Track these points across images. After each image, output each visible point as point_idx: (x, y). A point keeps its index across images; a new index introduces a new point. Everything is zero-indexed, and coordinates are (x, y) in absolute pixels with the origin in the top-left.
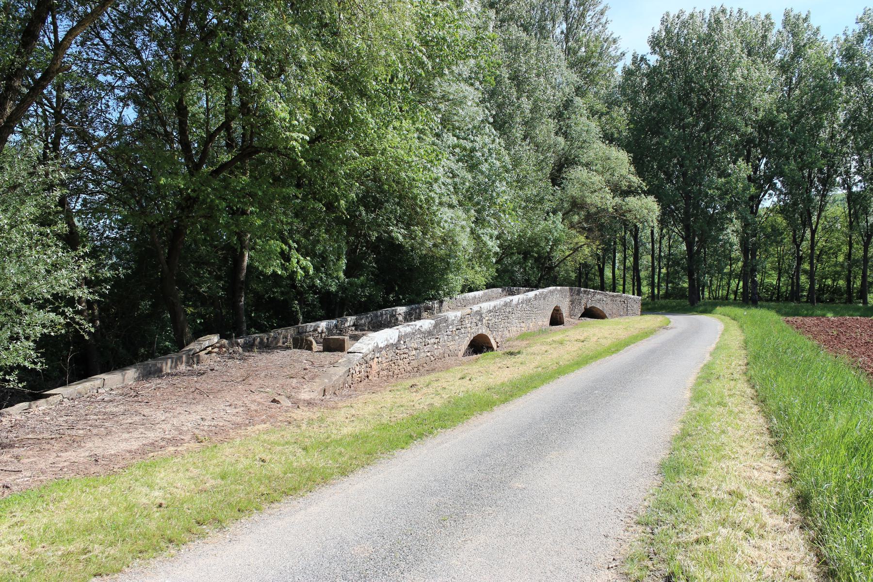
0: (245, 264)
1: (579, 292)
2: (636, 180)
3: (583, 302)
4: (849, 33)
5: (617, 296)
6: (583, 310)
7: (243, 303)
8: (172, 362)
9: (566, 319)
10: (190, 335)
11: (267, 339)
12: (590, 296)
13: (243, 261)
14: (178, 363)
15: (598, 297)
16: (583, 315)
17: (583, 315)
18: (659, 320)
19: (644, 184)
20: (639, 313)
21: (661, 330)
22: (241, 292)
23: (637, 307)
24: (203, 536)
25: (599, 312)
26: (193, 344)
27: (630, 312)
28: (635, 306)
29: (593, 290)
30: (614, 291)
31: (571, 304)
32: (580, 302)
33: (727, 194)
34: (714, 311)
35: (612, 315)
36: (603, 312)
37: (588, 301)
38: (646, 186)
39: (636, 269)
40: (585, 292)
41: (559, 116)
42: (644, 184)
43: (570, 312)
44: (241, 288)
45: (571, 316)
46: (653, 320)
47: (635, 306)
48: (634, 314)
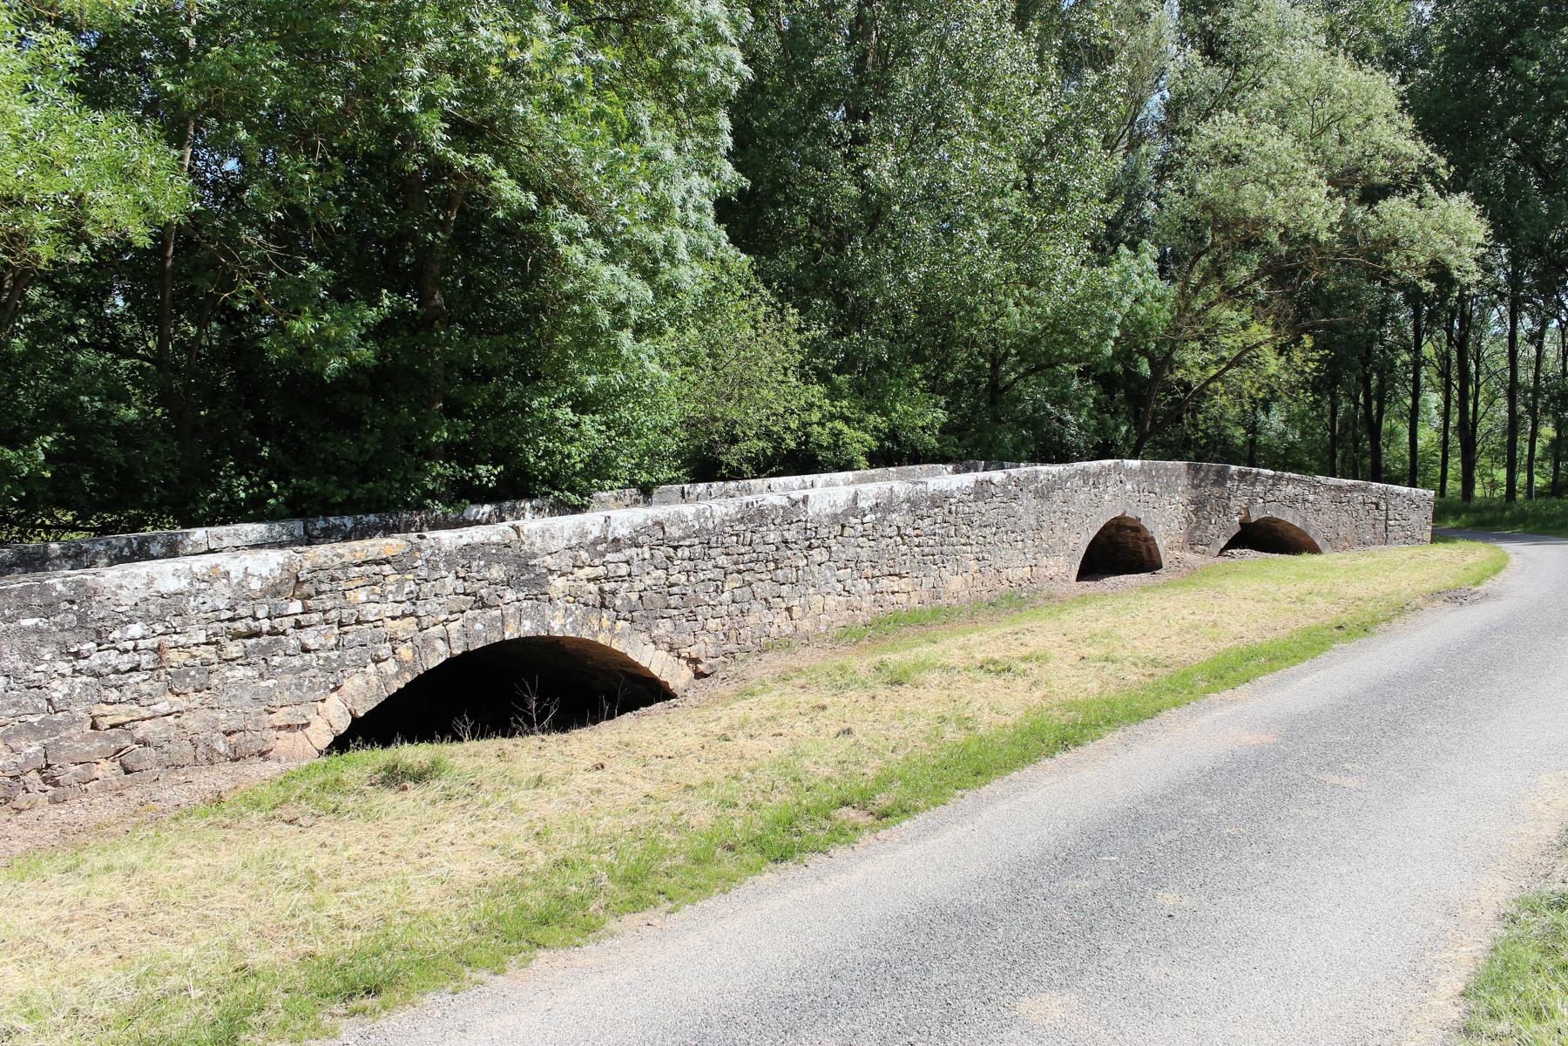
1: (1222, 478)
2: (1417, 151)
3: (1237, 504)
5: (1352, 489)
6: (1235, 529)
9: (1166, 557)
12: (1259, 488)
15: (1290, 490)
16: (1235, 543)
17: (1235, 543)
18: (1470, 559)
19: (1443, 161)
20: (1428, 536)
21: (1438, 603)
23: (1421, 520)
24: (727, 883)
27: (1397, 532)
28: (1414, 517)
29: (1270, 472)
30: (1413, 484)
31: (1195, 512)
35: (1336, 544)
36: (1305, 535)
37: (1252, 502)
38: (1447, 167)
39: (1467, 431)
40: (1242, 476)
41: (1372, 195)
42: (1443, 161)
43: (1191, 535)
45: (1192, 543)
46: (1470, 555)
47: (1414, 517)
48: (1410, 539)
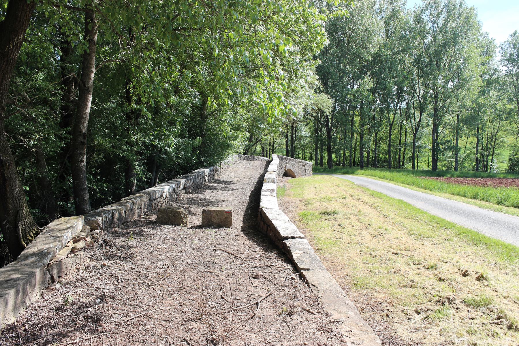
0: (88, 110)
4: (417, 7)
7: (84, 163)
8: (17, 293)
10: (30, 219)
11: (125, 212)
12: (287, 162)
13: (85, 106)
14: (29, 290)
15: (292, 162)
19: (322, 86)
22: (83, 149)
23: (310, 169)
25: (291, 173)
26: (41, 238)
32: (283, 166)
33: (358, 98)
34: (356, 173)
44: (83, 143)
48: (309, 174)
